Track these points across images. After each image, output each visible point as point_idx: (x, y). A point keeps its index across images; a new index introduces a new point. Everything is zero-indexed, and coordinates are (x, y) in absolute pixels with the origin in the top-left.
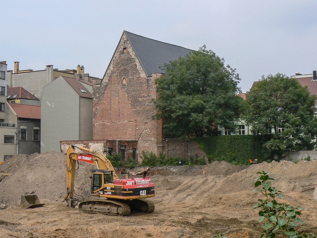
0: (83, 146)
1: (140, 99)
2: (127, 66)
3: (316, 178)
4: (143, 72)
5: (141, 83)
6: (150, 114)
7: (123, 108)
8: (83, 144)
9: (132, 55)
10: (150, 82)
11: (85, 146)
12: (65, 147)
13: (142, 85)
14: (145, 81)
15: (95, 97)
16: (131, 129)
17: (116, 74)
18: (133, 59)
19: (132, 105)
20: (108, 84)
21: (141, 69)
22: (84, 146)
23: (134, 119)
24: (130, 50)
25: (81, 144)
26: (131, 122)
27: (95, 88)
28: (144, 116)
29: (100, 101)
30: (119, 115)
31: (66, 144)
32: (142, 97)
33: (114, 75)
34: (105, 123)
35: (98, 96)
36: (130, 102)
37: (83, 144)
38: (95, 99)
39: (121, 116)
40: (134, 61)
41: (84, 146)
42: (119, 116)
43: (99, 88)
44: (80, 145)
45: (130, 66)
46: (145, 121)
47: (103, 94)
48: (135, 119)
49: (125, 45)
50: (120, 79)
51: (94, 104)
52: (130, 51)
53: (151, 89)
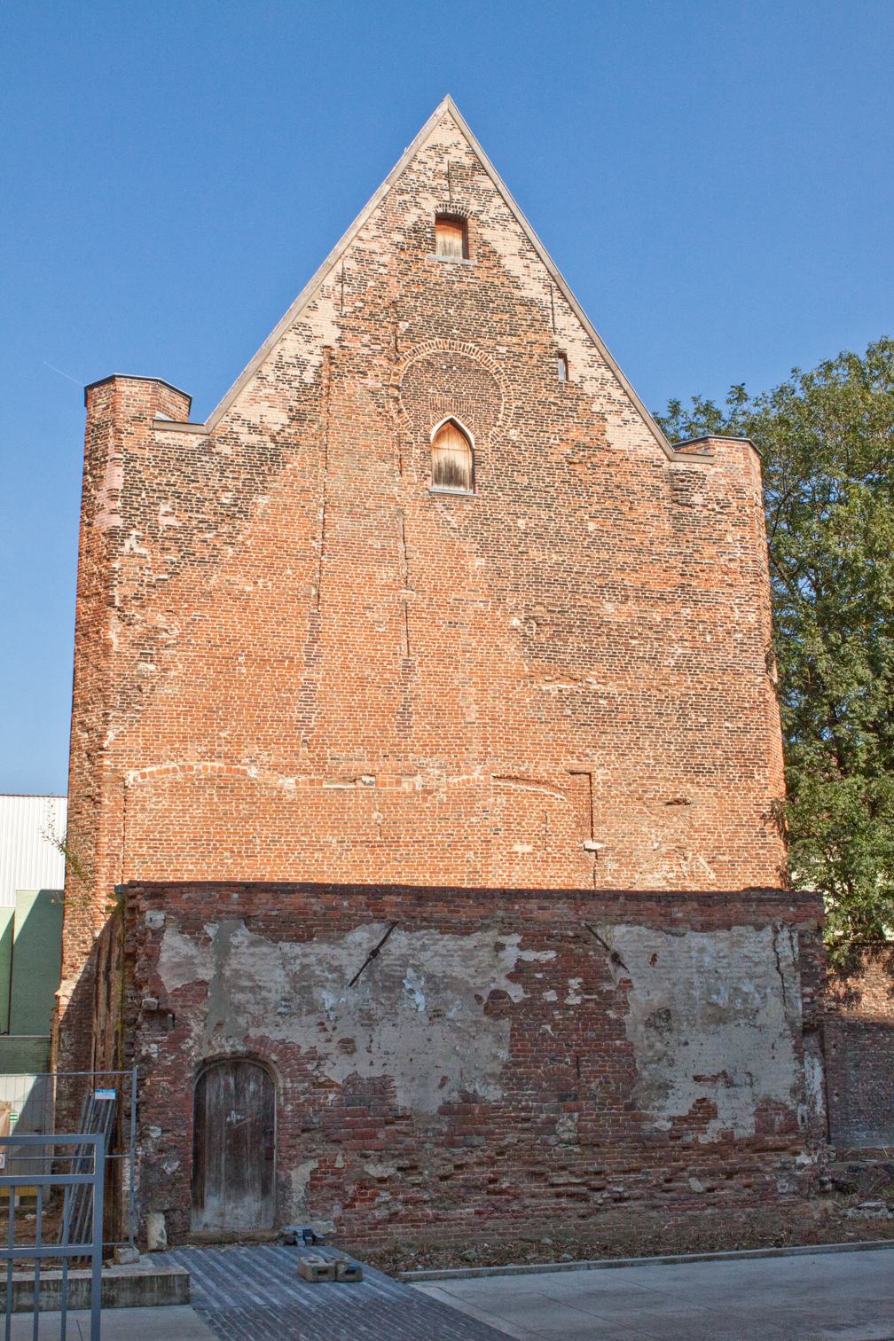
0: (511, 955)
1: (609, 607)
2: (478, 344)
3: (4, 1193)
4: (627, 414)
5: (617, 493)
6: (712, 734)
7: (443, 656)
8: (517, 939)
9: (523, 279)
10: (697, 499)
11: (551, 955)
12: (220, 967)
13: (625, 509)
14: (649, 481)
15: (134, 532)
16: (529, 849)
17: (370, 382)
18: (529, 304)
19: (534, 651)
20: (288, 445)
21: (608, 388)
22: (529, 956)
23: (557, 761)
24: (505, 240)
25: (490, 937)
26: (528, 781)
27: (147, 454)
28: (653, 745)
29: (190, 574)
30: (405, 713)
31: (247, 919)
32: (627, 598)
33: (352, 385)
34: (253, 772)
35: (170, 528)
36: (515, 622)
37: (517, 939)
38: (144, 551)
39: (419, 726)
40: (542, 322)
41: (529, 956)
42: (404, 726)
43: (185, 457)
44: (469, 942)
45: (503, 350)
46: (667, 789)
47: (233, 517)
48: (574, 763)
49: (456, 197)
50: (414, 431)
51: (130, 593)
52: (500, 247)
53: (710, 550)
